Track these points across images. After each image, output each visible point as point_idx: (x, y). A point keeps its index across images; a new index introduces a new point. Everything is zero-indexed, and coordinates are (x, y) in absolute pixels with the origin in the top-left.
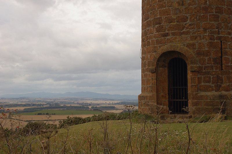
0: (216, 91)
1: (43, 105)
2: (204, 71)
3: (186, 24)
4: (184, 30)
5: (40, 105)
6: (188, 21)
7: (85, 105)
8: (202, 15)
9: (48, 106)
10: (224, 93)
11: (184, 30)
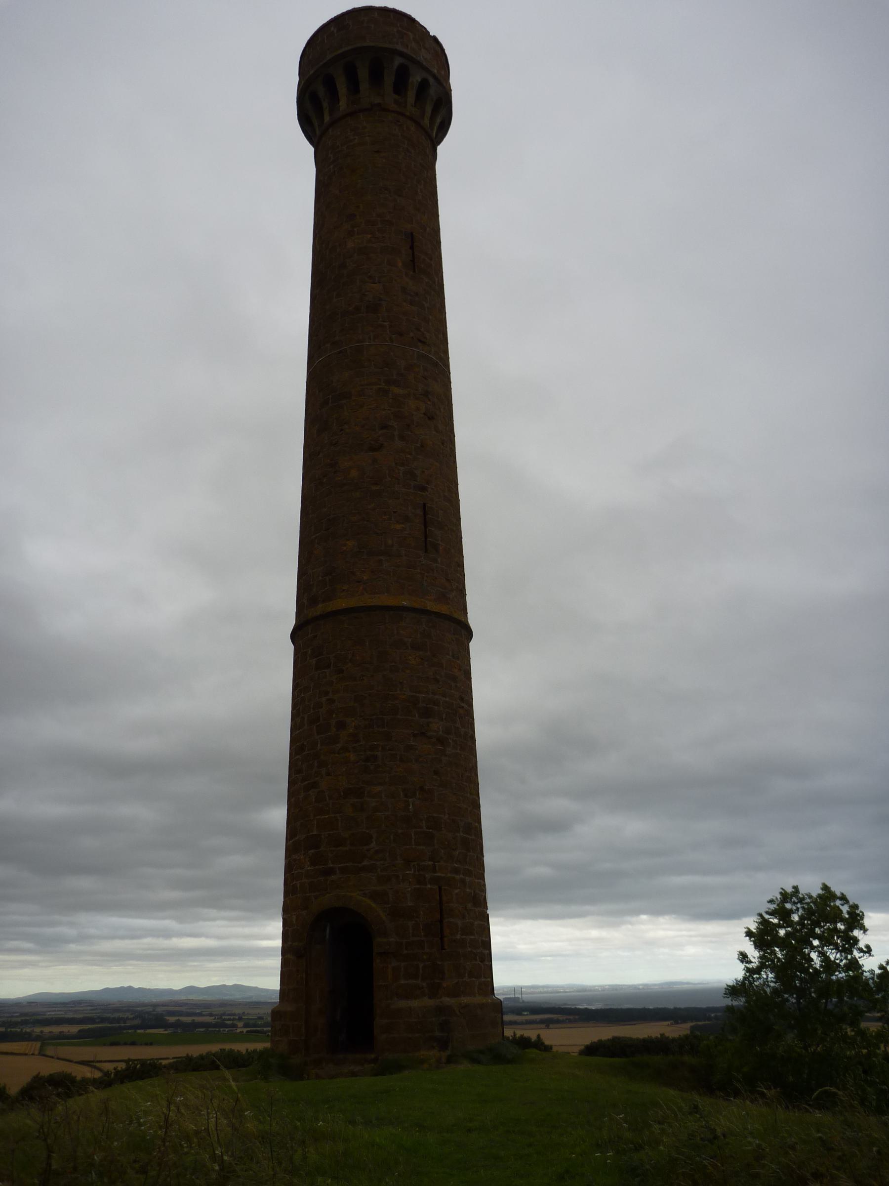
0: (430, 998)
1: (125, 1020)
2: (405, 952)
3: (368, 850)
4: (365, 863)
5: (119, 1020)
6: (373, 844)
7: (229, 1020)
8: (400, 831)
9: (137, 1022)
10: (447, 1000)
11: (365, 863)
